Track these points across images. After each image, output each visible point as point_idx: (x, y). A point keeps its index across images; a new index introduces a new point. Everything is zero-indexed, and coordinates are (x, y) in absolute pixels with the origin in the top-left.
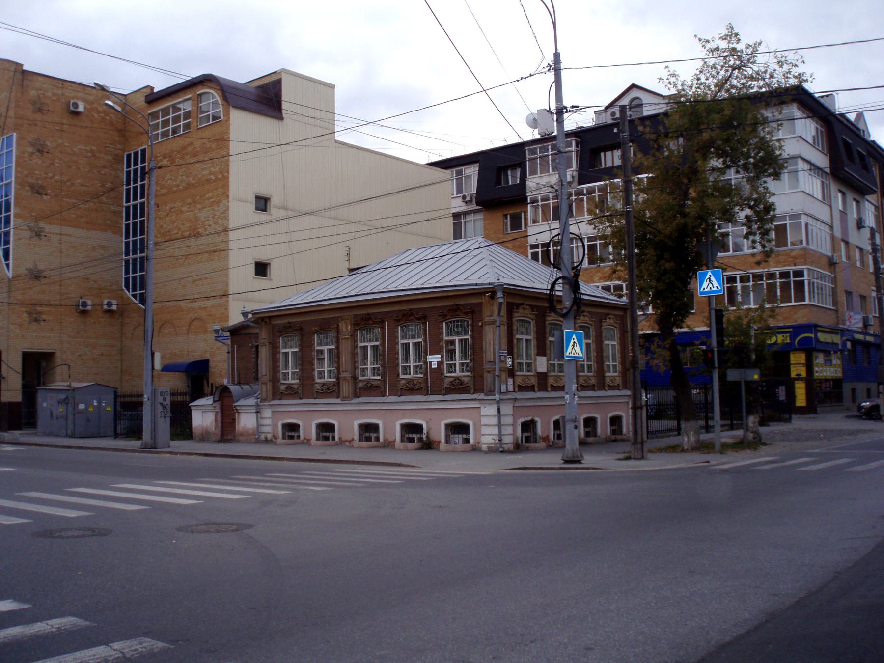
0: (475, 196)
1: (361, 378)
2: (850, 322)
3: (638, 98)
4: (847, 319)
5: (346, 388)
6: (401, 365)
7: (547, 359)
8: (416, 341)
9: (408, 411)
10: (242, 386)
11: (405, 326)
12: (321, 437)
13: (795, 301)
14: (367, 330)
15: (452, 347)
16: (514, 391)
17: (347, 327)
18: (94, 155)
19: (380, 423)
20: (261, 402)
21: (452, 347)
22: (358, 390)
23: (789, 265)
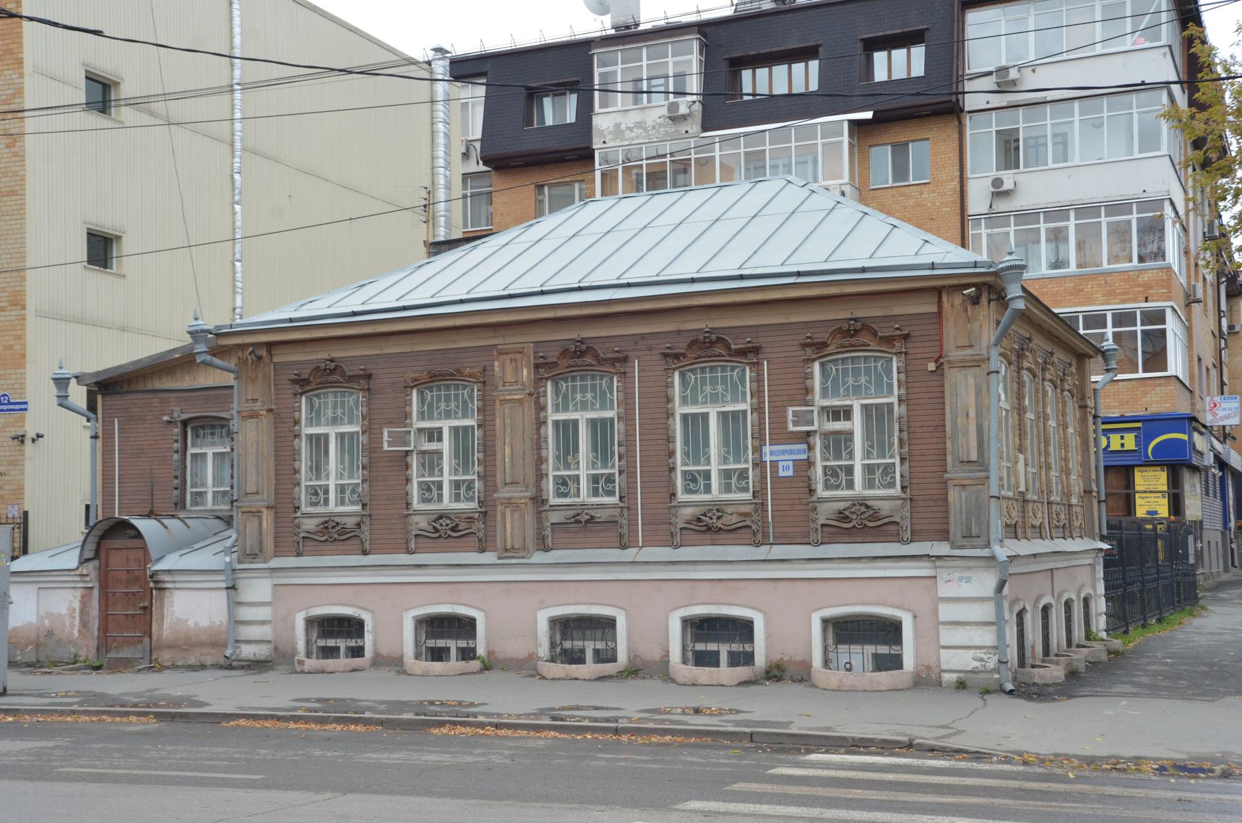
0: (478, 145)
1: (554, 501)
2: (1215, 415)
4: (1208, 408)
5: (511, 526)
6: (680, 468)
8: (729, 408)
9: (706, 584)
10: (166, 522)
11: (693, 371)
12: (315, 651)
13: (1145, 371)
14: (574, 379)
15: (433, 446)
17: (517, 371)
19: (366, 617)
20: (240, 562)
21: (433, 446)
22: (548, 532)
23: (1135, 300)
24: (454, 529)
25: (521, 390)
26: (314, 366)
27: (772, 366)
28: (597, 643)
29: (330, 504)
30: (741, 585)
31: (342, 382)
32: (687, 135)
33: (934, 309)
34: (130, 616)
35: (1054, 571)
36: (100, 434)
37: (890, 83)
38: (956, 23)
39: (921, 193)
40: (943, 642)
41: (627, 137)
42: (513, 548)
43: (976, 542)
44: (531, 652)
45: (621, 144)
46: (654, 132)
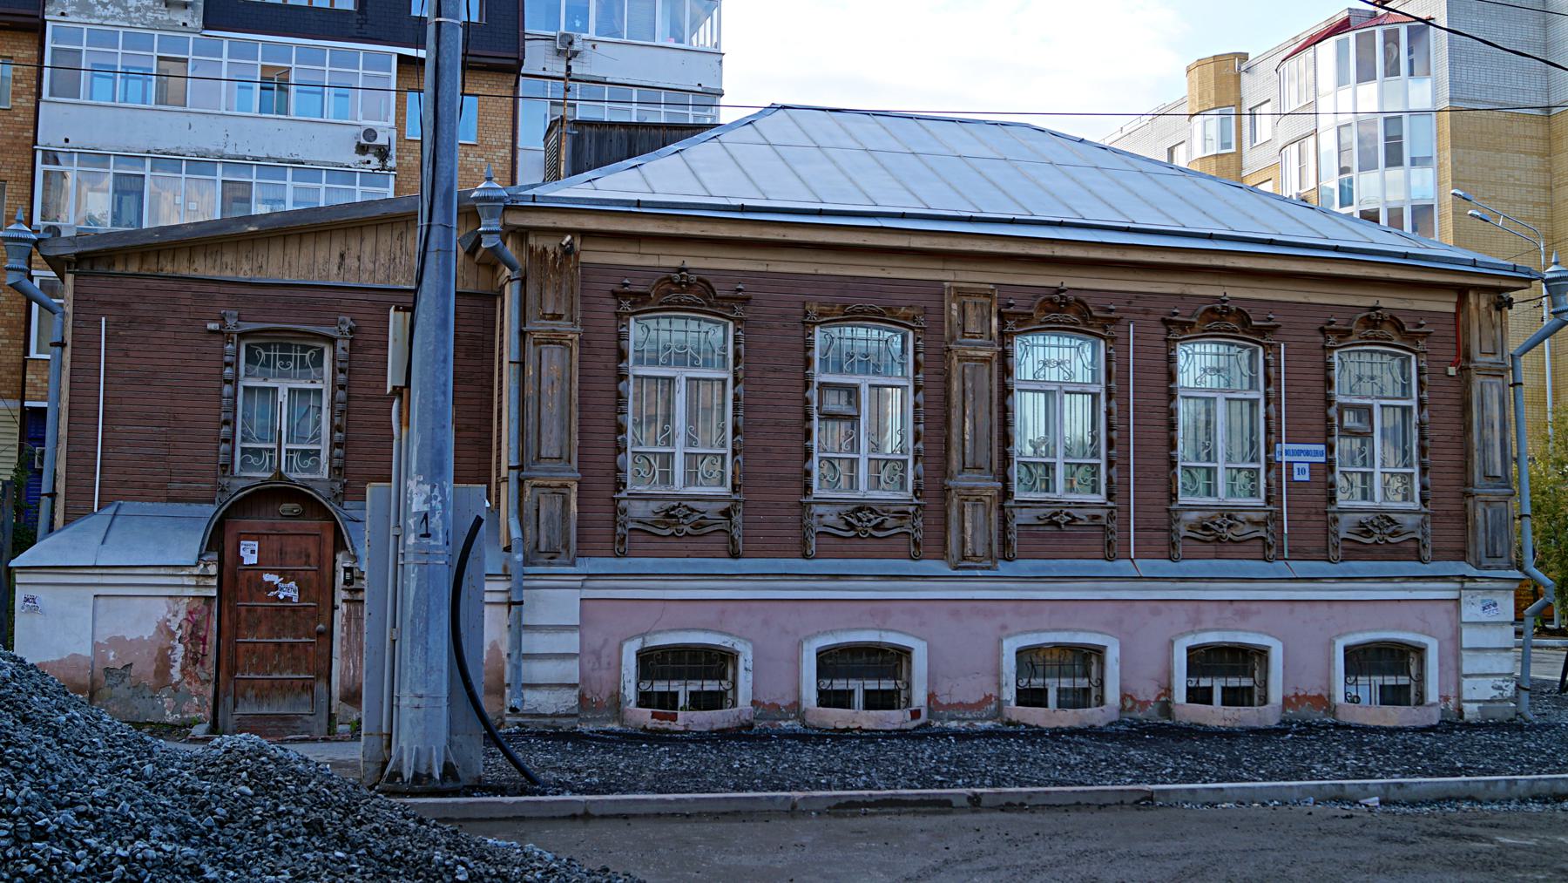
5: (975, 527)
9: (1325, 604)
24: (877, 527)
25: (988, 345)
26: (663, 276)
27: (1291, 351)
28: (1062, 680)
29: (676, 482)
31: (703, 305)
32: (184, 29)
33: (1452, 309)
34: (286, 647)
36: (69, 341)
39: (467, 155)
40: (1465, 671)
41: (97, 13)
42: (974, 555)
43: (1499, 562)
44: (988, 694)
45: (88, 21)
46: (137, 15)
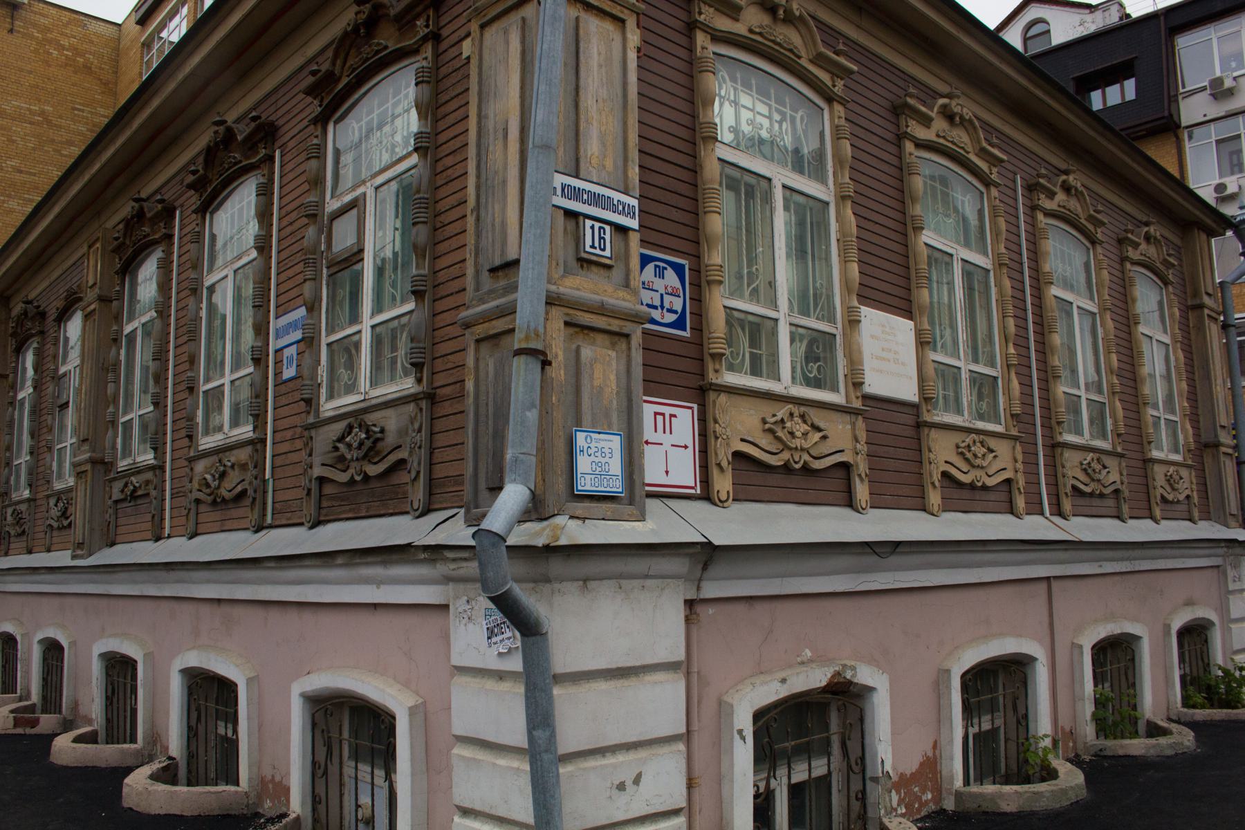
3: (1040, 21)
7: (919, 333)
16: (707, 495)
18: (49, 122)
30: (238, 611)
35: (1055, 584)
37: (1106, 109)
38: (1164, 47)
